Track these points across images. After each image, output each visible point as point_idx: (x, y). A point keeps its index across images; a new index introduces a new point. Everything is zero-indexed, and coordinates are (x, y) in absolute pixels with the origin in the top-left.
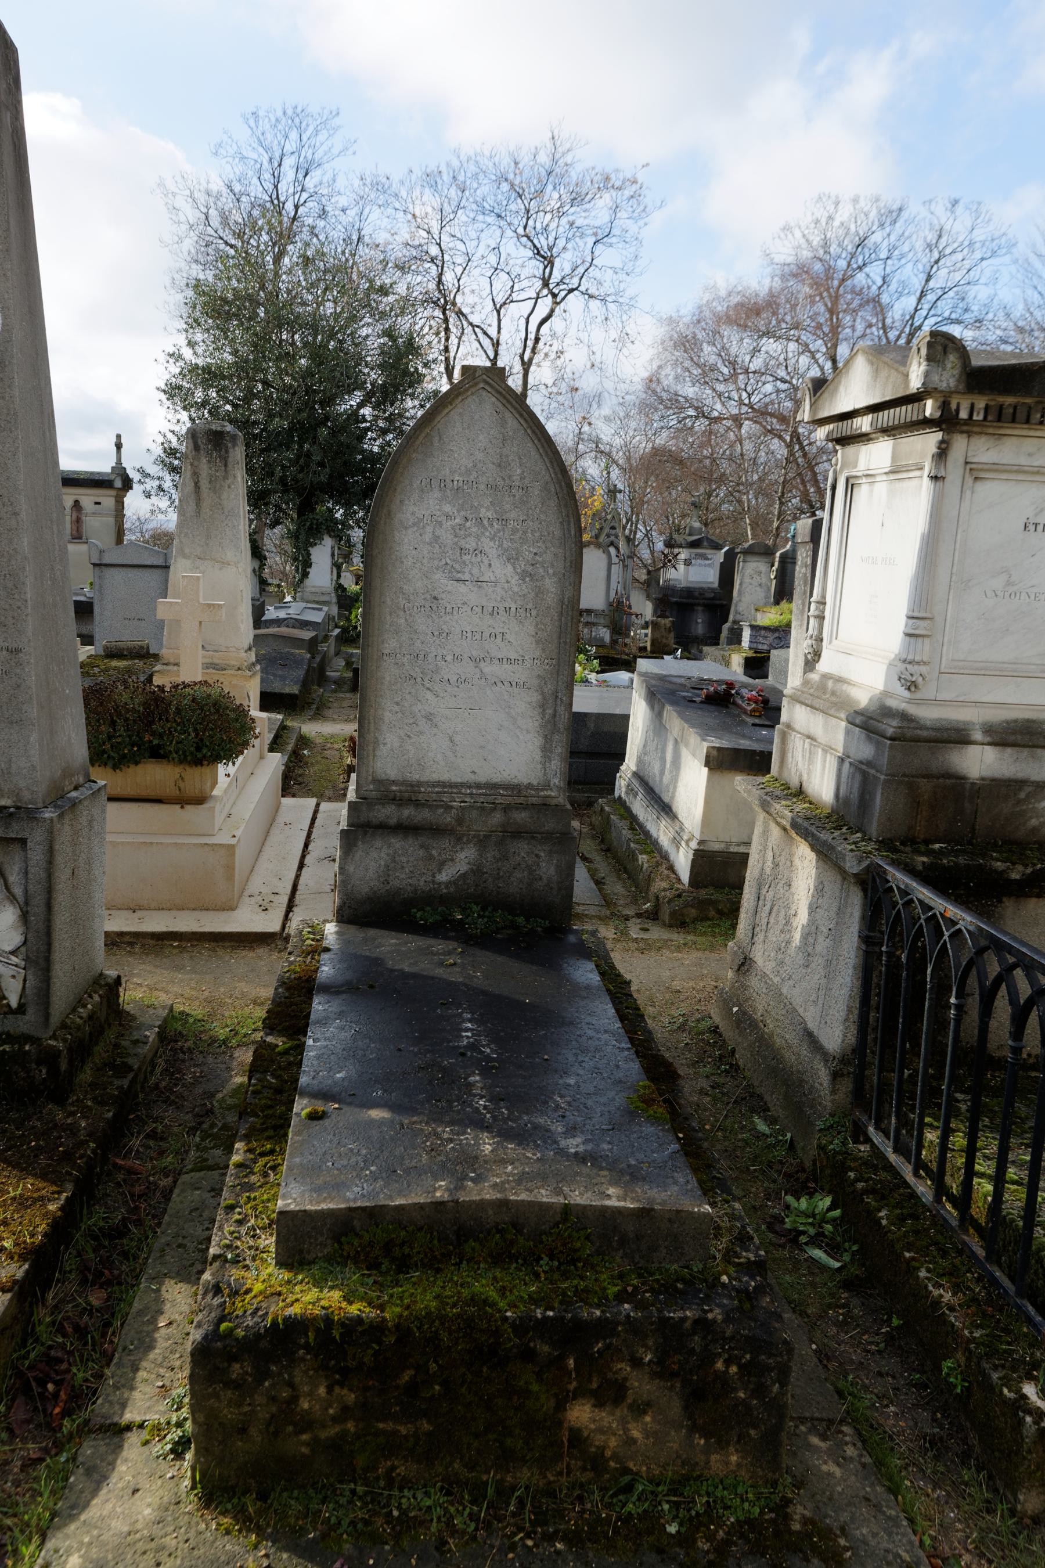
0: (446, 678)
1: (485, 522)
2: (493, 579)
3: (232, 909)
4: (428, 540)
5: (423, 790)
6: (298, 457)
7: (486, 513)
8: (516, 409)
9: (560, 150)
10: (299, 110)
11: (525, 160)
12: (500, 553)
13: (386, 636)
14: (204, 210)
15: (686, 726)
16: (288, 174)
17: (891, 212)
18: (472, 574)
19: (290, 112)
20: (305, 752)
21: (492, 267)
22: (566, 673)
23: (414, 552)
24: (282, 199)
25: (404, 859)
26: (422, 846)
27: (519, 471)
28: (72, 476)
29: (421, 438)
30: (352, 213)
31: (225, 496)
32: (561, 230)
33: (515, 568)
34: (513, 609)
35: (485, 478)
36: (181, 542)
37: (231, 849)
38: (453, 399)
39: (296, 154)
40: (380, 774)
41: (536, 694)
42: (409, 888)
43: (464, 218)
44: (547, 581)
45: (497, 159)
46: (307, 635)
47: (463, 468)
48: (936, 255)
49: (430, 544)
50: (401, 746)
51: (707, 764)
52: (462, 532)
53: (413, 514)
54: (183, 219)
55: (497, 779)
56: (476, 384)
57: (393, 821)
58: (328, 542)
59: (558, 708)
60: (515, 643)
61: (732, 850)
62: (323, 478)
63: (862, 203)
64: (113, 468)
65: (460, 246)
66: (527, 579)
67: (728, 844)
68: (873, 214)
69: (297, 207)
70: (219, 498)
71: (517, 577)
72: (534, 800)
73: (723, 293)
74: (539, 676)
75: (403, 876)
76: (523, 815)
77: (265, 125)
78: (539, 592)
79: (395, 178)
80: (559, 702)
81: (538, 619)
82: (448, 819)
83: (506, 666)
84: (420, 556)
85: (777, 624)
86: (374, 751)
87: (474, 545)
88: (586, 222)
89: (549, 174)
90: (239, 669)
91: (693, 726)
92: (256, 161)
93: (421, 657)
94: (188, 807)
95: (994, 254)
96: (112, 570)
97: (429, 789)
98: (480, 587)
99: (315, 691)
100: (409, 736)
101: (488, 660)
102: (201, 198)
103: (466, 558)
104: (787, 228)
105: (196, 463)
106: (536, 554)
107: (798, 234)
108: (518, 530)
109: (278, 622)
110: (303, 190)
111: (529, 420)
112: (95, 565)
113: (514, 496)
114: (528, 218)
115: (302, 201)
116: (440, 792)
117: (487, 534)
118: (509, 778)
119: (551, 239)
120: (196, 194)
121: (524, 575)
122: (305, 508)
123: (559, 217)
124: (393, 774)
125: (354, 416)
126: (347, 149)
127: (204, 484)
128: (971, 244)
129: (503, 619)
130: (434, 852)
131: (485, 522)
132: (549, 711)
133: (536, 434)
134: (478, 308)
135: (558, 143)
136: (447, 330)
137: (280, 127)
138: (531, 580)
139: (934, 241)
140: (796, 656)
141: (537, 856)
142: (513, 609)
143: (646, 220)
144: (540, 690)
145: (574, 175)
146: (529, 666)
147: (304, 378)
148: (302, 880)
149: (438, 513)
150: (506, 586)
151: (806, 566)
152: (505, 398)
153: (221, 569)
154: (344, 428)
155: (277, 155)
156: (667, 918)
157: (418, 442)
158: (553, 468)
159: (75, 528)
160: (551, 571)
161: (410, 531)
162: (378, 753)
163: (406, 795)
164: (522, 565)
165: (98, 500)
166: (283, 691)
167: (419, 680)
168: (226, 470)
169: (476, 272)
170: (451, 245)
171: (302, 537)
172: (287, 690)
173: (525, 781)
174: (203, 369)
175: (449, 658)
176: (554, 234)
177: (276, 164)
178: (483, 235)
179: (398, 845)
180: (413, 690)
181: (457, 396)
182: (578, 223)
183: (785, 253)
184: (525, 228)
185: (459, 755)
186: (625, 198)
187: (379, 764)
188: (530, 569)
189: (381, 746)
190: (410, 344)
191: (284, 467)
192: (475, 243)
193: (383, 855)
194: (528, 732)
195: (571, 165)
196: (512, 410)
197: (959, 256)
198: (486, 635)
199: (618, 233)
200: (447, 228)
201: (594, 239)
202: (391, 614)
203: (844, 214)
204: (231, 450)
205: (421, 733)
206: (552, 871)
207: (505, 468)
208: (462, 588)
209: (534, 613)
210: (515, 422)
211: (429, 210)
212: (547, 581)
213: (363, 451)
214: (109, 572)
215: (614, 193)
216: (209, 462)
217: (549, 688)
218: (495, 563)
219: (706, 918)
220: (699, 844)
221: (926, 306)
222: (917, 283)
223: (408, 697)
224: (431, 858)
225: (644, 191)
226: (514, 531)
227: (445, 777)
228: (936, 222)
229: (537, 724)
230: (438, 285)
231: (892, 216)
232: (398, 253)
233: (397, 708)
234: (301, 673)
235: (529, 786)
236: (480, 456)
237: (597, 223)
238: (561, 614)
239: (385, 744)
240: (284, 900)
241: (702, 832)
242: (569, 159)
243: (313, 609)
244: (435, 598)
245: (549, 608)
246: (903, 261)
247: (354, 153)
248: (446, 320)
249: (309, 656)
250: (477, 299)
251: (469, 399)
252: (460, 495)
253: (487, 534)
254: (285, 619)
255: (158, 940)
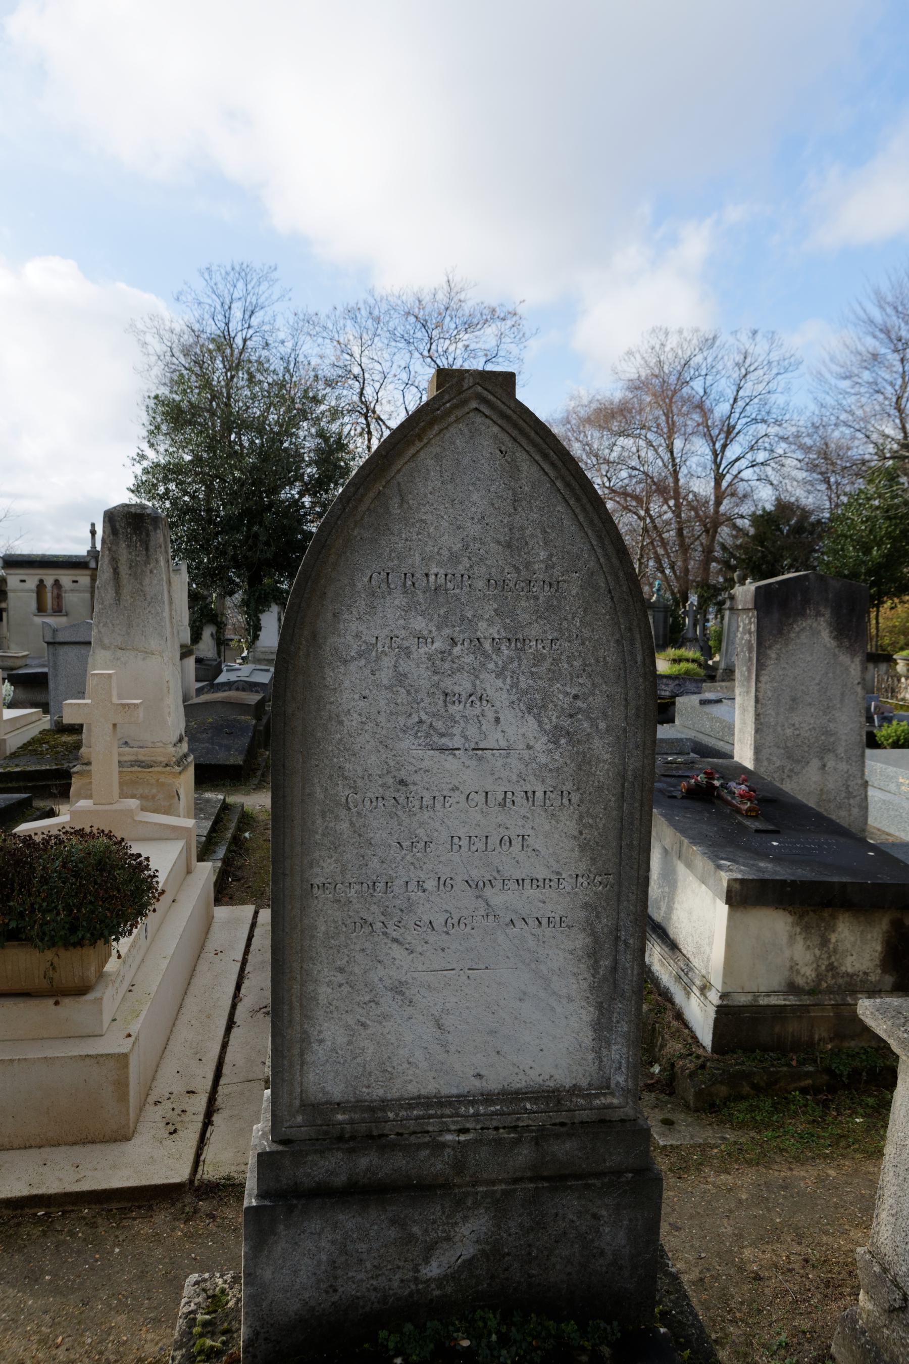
0: (426, 919)
1: (487, 646)
2: (503, 744)
3: (126, 1138)
4: (385, 682)
5: (391, 1115)
6: (247, 538)
7: (486, 630)
8: (535, 445)
9: (455, 291)
10: (245, 266)
11: (427, 299)
12: (514, 698)
13: (316, 855)
14: (169, 344)
15: (686, 841)
16: (237, 313)
17: (707, 340)
18: (466, 738)
19: (237, 268)
20: (247, 835)
21: (403, 382)
22: (633, 897)
23: (362, 703)
24: (232, 335)
25: (363, 1247)
26: (393, 1222)
27: (543, 555)
28: (52, 559)
29: (367, 501)
30: (289, 345)
31: (147, 581)
32: (458, 352)
33: (540, 724)
34: (539, 795)
35: (484, 569)
36: (99, 632)
37: (122, 1059)
38: (424, 430)
39: (243, 299)
40: (314, 1093)
41: (582, 936)
42: (373, 1296)
43: (380, 345)
44: (597, 743)
45: (404, 298)
46: (253, 698)
47: (445, 552)
48: (743, 371)
49: (389, 688)
50: (350, 1043)
51: (729, 901)
52: (447, 665)
53: (358, 636)
54: (151, 351)
55: (519, 1082)
56: (464, 402)
57: (340, 1180)
58: (275, 609)
59: (622, 958)
60: (543, 851)
61: (761, 1002)
62: (269, 555)
63: (685, 334)
64: (88, 552)
65: (378, 367)
66: (563, 741)
67: (756, 995)
68: (695, 341)
69: (245, 341)
70: (141, 584)
71: (545, 739)
72: (585, 1115)
73: (585, 401)
74: (586, 905)
75: (362, 1276)
76: (568, 1145)
77: (217, 277)
78: (584, 762)
79: (322, 316)
80: (621, 947)
81: (583, 808)
82: (439, 1166)
83: (530, 892)
84: (374, 710)
85: (677, 673)
86: (302, 1054)
87: (468, 686)
88: (478, 346)
89: (447, 309)
90: (167, 765)
91: (694, 841)
92: (211, 306)
93: (380, 886)
94: (66, 1001)
95: (786, 370)
96: (66, 648)
97: (403, 1113)
98: (481, 759)
99: (262, 755)
100: (363, 1025)
101: (498, 884)
102: (167, 335)
103: (454, 709)
104: (630, 353)
105: (114, 548)
106: (576, 697)
107: (638, 356)
108: (544, 657)
109: (229, 685)
110: (249, 327)
111: (559, 464)
112: (48, 643)
113: (536, 598)
114: (431, 344)
115: (249, 336)
116: (423, 1117)
117: (491, 666)
118: (540, 1080)
119: (451, 359)
120: (162, 332)
121: (556, 735)
122: (254, 580)
123: (456, 343)
124: (337, 1091)
125: (296, 503)
126: (284, 296)
127: (124, 570)
128: (769, 363)
129: (523, 811)
130: (416, 1229)
131: (487, 646)
132: (605, 963)
133: (572, 490)
134: (394, 415)
135: (452, 285)
136: (369, 433)
137: (229, 279)
138: (569, 742)
139: (741, 361)
140: (744, 723)
141: (595, 1216)
142: (539, 795)
143: (526, 344)
144: (590, 928)
145: (467, 308)
146: (568, 889)
147: (250, 472)
148: (229, 1058)
149: (403, 633)
150: (526, 754)
151: (750, 633)
152: (516, 426)
153: (144, 659)
154: (286, 514)
155: (227, 302)
156: (691, 1099)
157: (363, 508)
158: (603, 547)
159: (56, 603)
160: (602, 725)
161: (353, 667)
162: (309, 1058)
163: (363, 1128)
164: (552, 718)
165: (75, 579)
166: (228, 763)
167: (378, 926)
168: (148, 556)
169: (390, 387)
170: (370, 366)
171: (253, 605)
172: (232, 761)
173: (568, 1083)
174: (164, 467)
175: (430, 885)
176: (453, 355)
177: (227, 307)
178: (395, 357)
179: (349, 1225)
180: (368, 945)
181: (431, 424)
182: (472, 347)
183: (633, 370)
184: (429, 351)
185: (452, 1049)
186: (507, 327)
187: (311, 1076)
188: (566, 723)
189: (315, 1046)
190: (342, 447)
191: (235, 547)
192: (389, 364)
193: (323, 1244)
194: (570, 999)
195: (464, 301)
196: (529, 448)
197: (761, 372)
198: (494, 840)
199: (503, 354)
200: (366, 353)
201: (484, 359)
202: (323, 815)
203: (672, 342)
204: (152, 534)
205: (385, 1017)
206: (621, 1238)
207: (519, 550)
208: (450, 763)
209: (575, 798)
210: (535, 468)
211: (351, 338)
212: (597, 743)
213: (303, 532)
214: (62, 650)
215: (499, 324)
216: (129, 546)
217: (604, 923)
218: (507, 716)
219: (741, 1098)
220: (721, 997)
221: (738, 410)
222: (730, 393)
223: (359, 957)
224: (410, 1239)
225: (524, 322)
226: (538, 659)
227: (430, 1087)
228: (742, 347)
229: (585, 985)
230: (360, 398)
231: (709, 342)
232: (328, 372)
233: (340, 978)
234: (245, 741)
235: (575, 1090)
236: (474, 530)
237: (487, 346)
238: (622, 797)
239: (321, 1041)
240: (200, 1103)
241: (724, 983)
242: (462, 296)
243: (262, 670)
244: (402, 782)
245: (600, 788)
246: (718, 377)
247: (290, 299)
248: (368, 425)
249: (254, 722)
250: (392, 409)
251: (453, 430)
252: (441, 600)
253: (491, 666)
254: (236, 682)
255: (15, 1209)
